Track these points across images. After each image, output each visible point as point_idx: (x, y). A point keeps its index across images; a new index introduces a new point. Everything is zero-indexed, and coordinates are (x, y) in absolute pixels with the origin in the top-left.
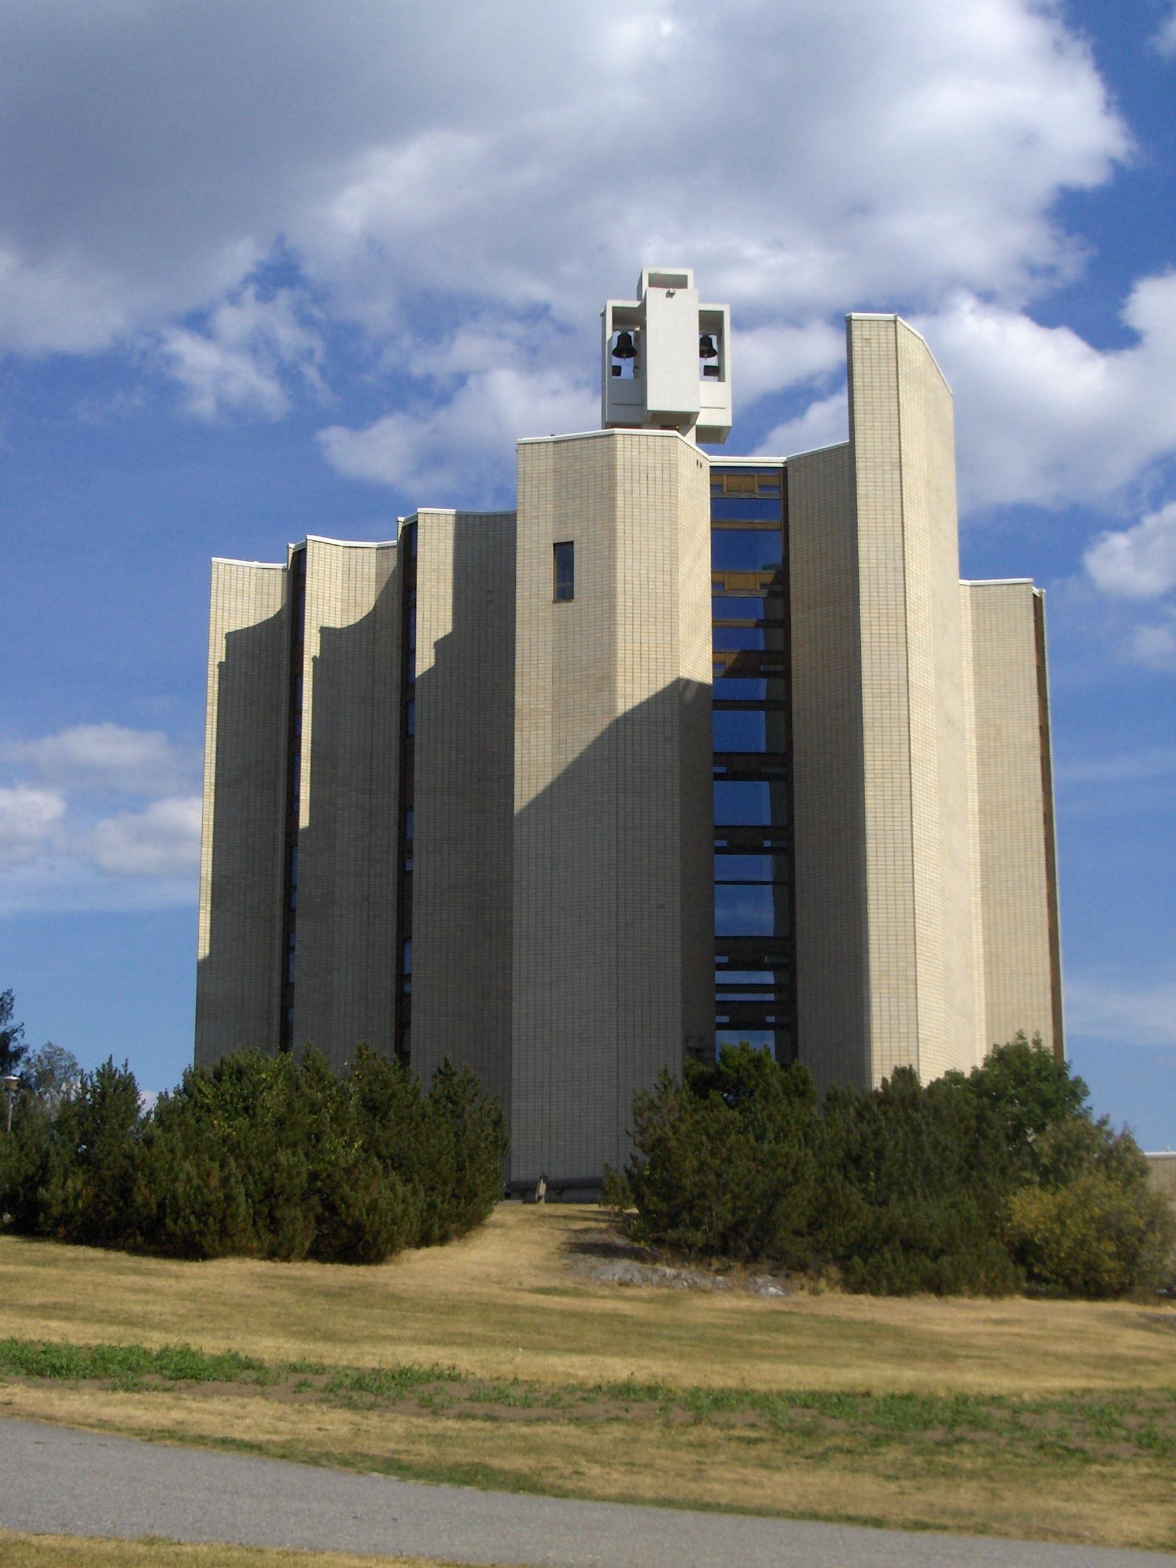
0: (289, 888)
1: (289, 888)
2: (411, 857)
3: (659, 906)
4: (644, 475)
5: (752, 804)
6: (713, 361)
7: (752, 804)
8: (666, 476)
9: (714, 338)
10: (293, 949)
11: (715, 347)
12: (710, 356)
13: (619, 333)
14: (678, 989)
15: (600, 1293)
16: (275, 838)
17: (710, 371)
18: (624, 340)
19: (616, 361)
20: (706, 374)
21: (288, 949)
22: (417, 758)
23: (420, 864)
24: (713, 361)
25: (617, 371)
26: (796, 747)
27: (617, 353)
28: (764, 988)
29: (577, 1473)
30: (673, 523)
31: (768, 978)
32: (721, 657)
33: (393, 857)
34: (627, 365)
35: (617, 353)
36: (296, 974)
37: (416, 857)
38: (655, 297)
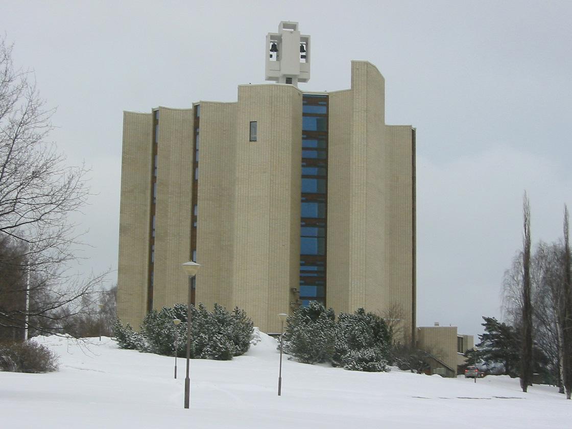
0: (152, 229)
1: (152, 229)
2: (196, 221)
5: (313, 210)
6: (304, 54)
7: (313, 210)
10: (153, 251)
13: (272, 44)
14: (288, 273)
16: (146, 211)
17: (303, 57)
19: (271, 53)
20: (188, 408)
21: (151, 251)
22: (199, 188)
23: (198, 224)
24: (304, 54)
25: (271, 56)
26: (328, 191)
30: (198, 353)
31: (315, 268)
32: (14, 370)
33: (189, 222)
34: (274, 54)
35: (271, 51)
36: (155, 260)
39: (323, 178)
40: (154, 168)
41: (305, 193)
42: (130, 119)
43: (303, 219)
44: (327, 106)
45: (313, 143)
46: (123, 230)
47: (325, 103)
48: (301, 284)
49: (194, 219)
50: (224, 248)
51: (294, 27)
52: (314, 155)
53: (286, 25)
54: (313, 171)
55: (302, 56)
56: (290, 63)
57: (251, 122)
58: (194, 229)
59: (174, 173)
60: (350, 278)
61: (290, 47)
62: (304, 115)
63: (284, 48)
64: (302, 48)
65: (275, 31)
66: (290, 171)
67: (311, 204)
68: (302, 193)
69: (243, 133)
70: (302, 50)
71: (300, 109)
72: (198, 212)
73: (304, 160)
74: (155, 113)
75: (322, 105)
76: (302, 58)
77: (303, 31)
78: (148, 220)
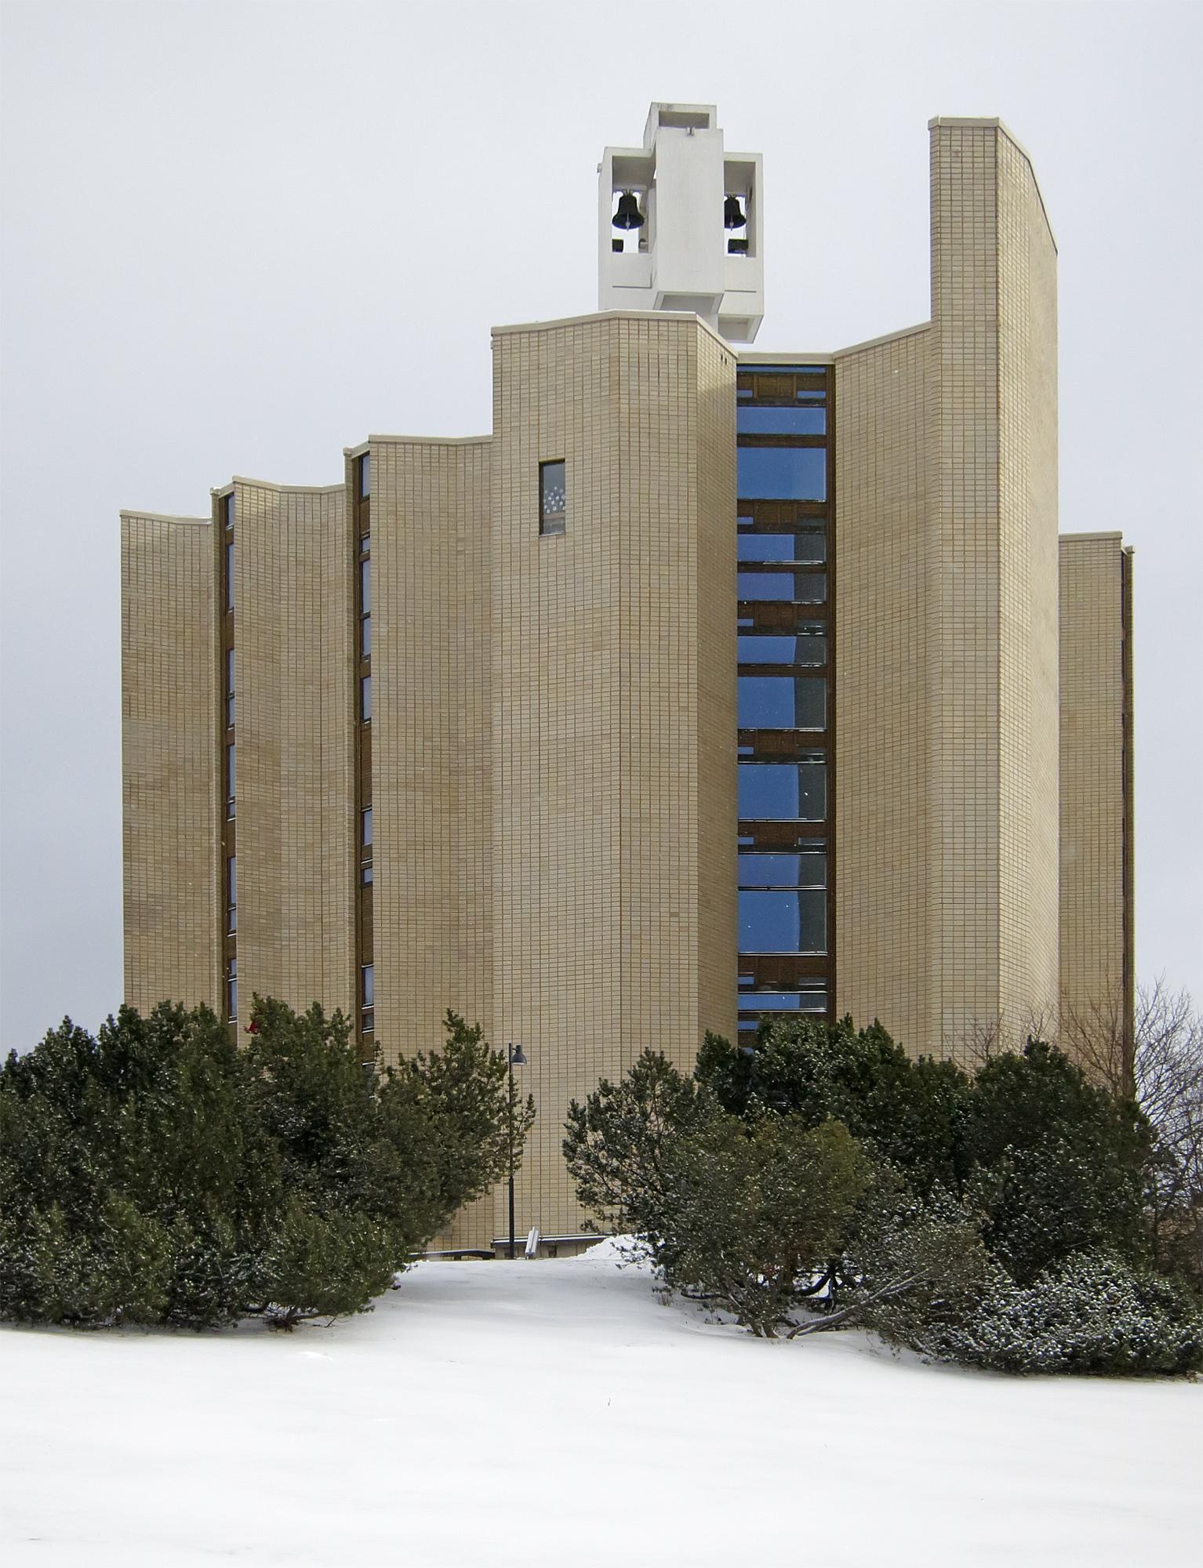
3: (672, 915)
4: (654, 370)
5: (781, 793)
6: (739, 233)
7: (781, 793)
8: (683, 371)
9: (742, 201)
11: (743, 212)
12: (737, 225)
13: (620, 194)
15: (802, 395)
17: (736, 246)
18: (627, 202)
19: (618, 233)
22: (375, 746)
24: (739, 233)
25: (618, 246)
27: (619, 221)
28: (820, 987)
29: (308, 1146)
34: (630, 237)
35: (619, 221)
37: (376, 867)
38: (672, 143)
39: (817, 678)
40: (226, 698)
41: (753, 604)
42: (145, 547)
43: (744, 736)
44: (829, 405)
45: (780, 547)
46: (136, 913)
47: (822, 395)
48: (742, 631)
49: (362, 853)
50: (471, 952)
51: (698, 120)
52: (780, 589)
53: (669, 118)
54: (781, 648)
55: (731, 241)
56: (686, 243)
57: (542, 465)
58: (363, 889)
59: (295, 706)
60: (935, 999)
61: (687, 197)
62: (745, 440)
63: (664, 206)
64: (731, 207)
65: (632, 141)
66: (694, 640)
67: (776, 769)
68: (740, 502)
69: (520, 500)
70: (733, 217)
71: (733, 648)
72: (374, 835)
73: (745, 608)
74: (223, 504)
75: (808, 402)
76: (731, 251)
77: (736, 138)
78: (215, 877)
